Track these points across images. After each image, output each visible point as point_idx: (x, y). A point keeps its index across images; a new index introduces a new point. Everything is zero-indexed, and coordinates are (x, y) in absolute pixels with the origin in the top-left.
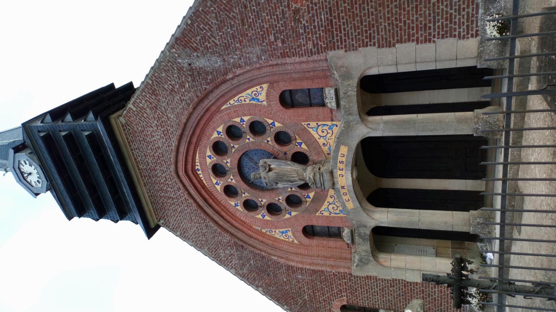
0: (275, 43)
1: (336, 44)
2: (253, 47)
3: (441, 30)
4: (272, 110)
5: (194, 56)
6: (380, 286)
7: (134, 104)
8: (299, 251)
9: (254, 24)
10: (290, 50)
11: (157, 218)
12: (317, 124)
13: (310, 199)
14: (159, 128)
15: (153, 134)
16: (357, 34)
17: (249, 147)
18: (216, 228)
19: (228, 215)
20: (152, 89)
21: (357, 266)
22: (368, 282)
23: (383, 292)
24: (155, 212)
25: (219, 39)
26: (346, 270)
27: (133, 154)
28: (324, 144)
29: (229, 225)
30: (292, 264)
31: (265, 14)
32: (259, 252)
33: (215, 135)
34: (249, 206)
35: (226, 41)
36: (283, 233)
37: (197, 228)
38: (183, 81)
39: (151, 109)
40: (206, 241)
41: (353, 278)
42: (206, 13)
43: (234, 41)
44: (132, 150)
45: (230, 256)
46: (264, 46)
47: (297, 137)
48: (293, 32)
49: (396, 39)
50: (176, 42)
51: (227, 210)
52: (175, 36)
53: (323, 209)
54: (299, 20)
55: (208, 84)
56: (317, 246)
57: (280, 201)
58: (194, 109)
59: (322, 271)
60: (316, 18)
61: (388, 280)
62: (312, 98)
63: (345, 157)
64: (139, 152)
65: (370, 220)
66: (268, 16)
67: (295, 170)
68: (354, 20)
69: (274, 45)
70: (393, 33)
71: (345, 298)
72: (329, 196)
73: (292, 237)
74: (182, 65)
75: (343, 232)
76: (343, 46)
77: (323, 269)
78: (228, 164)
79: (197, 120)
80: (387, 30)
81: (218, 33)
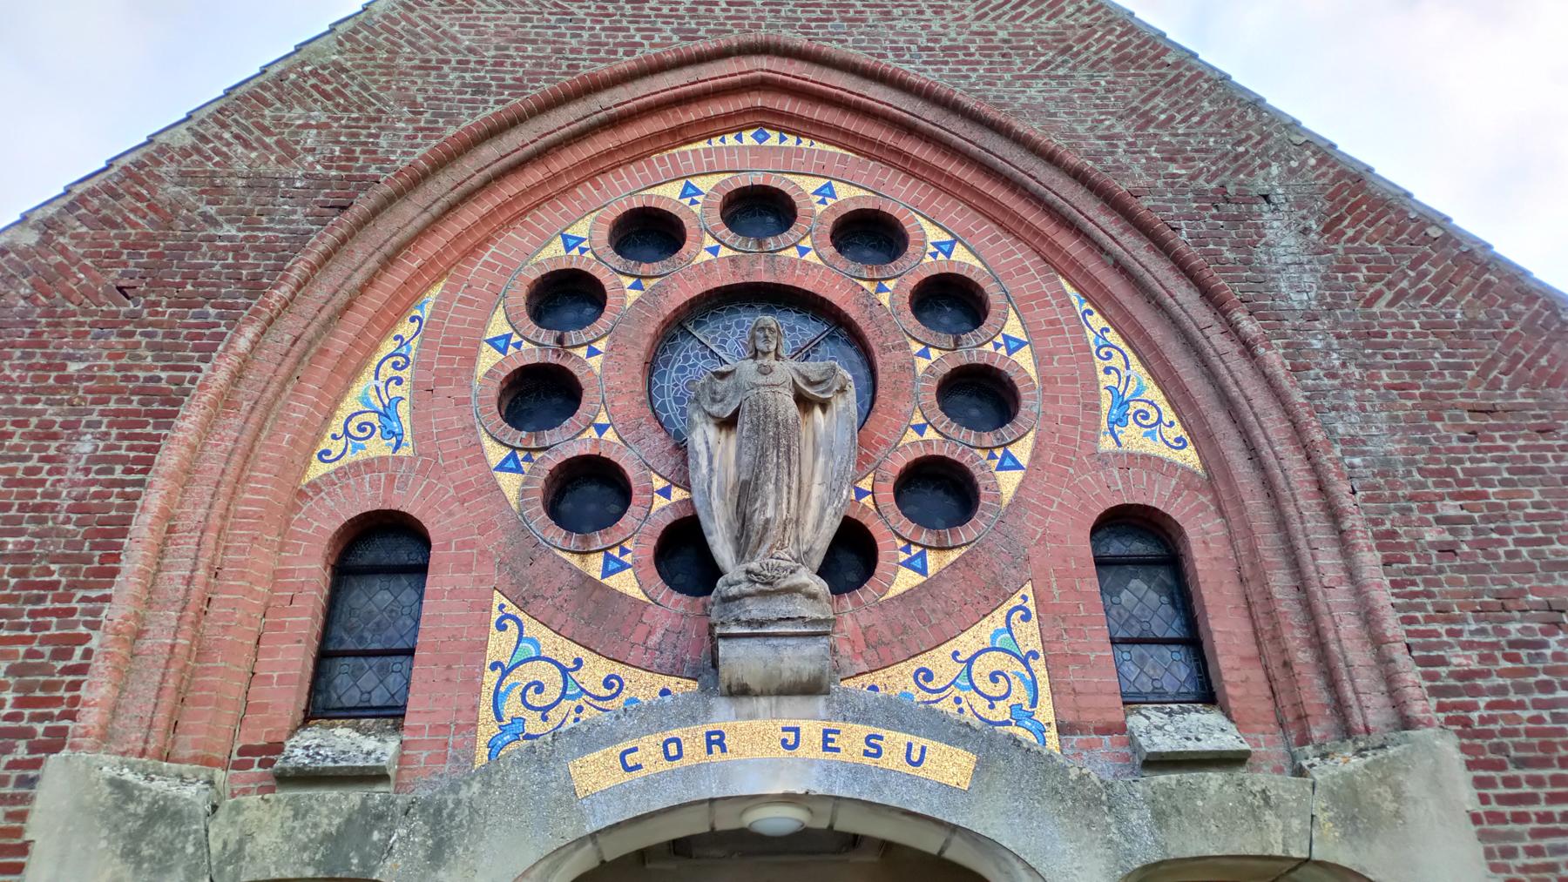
1: (1497, 775)
2: (1392, 431)
4: (1081, 467)
8: (262, 474)
13: (598, 576)
14: (977, 39)
15: (948, 15)
17: (885, 349)
18: (467, 122)
19: (525, 193)
21: (118, 785)
26: (91, 718)
29: (477, 180)
30: (189, 421)
32: (295, 275)
33: (933, 234)
34: (565, 296)
35: (1390, 338)
37: (471, 50)
39: (1059, 36)
40: (388, 69)
41: (21, 751)
46: (1409, 473)
47: (953, 556)
51: (549, 198)
53: (533, 628)
55: (1199, 241)
56: (277, 574)
59: (114, 572)
62: (1137, 650)
72: (618, 669)
73: (350, 458)
76: (1494, 806)
77: (127, 584)
78: (793, 253)
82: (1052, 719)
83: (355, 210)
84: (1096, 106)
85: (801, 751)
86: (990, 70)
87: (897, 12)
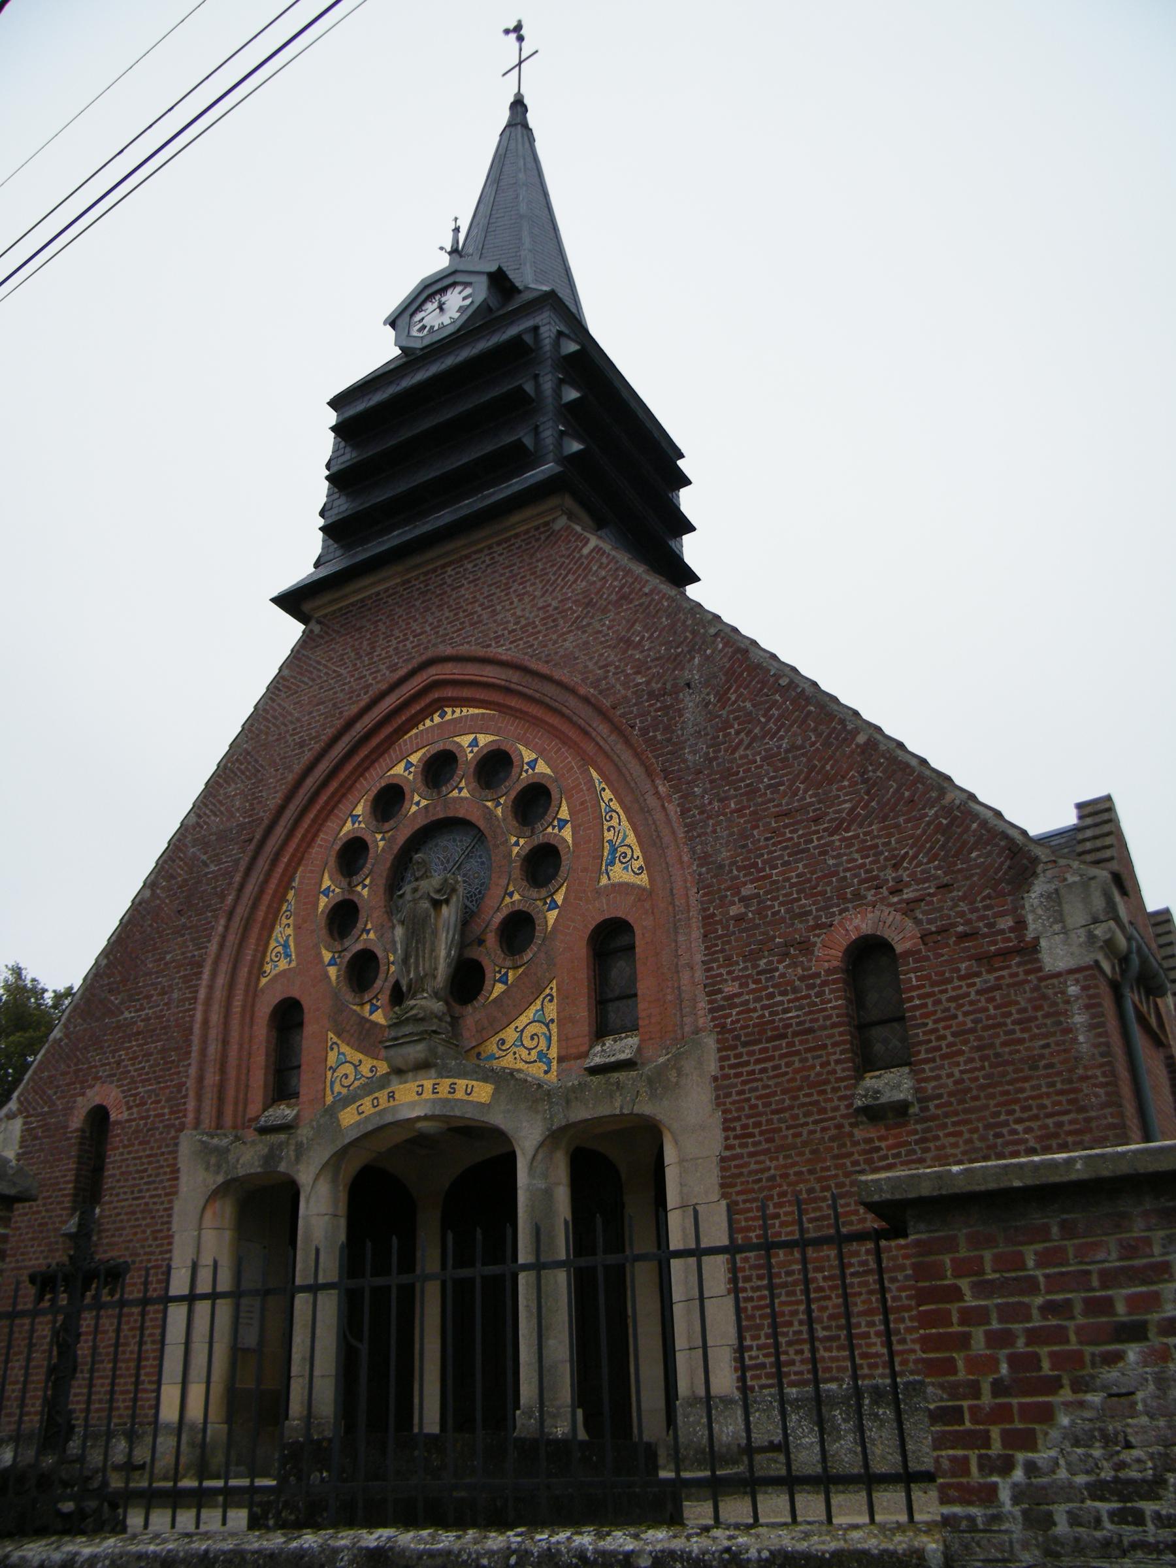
0: (736, 899)
3: (755, 1303)
5: (708, 694)
6: (155, 1203)
7: (597, 549)
9: (780, 842)
10: (720, 937)
11: (325, 616)
12: (552, 1021)
13: (367, 1015)
15: (526, 599)
16: (753, 1101)
20: (630, 593)
21: (203, 1142)
22: (165, 1173)
23: (142, 1212)
24: (340, 609)
25: (747, 756)
27: (480, 551)
28: (503, 1042)
31: (801, 870)
33: (528, 755)
36: (286, 946)
37: (298, 720)
38: (649, 668)
41: (173, 1133)
42: (804, 721)
43: (741, 795)
44: (490, 547)
45: (228, 810)
46: (731, 871)
47: (521, 970)
48: (761, 942)
49: (740, 1198)
50: (739, 650)
52: (752, 648)
53: (345, 1048)
54: (787, 954)
55: (644, 732)
57: (364, 936)
58: (586, 700)
60: (791, 996)
61: (169, 1223)
63: (466, 1097)
64: (483, 566)
65: (314, 1169)
66: (798, 876)
67: (436, 969)
68: (784, 1092)
69: (732, 895)
70: (753, 1191)
71: (125, 1116)
72: (375, 1062)
73: (274, 972)
74: (688, 666)
75: (288, 1106)
76: (727, 1070)
78: (455, 793)
79: (560, 707)
80: (759, 1176)
81: (760, 753)
82: (555, 1055)
83: (255, 841)
84: (601, 643)
85: (424, 1096)
86: (545, 636)
87: (499, 607)
